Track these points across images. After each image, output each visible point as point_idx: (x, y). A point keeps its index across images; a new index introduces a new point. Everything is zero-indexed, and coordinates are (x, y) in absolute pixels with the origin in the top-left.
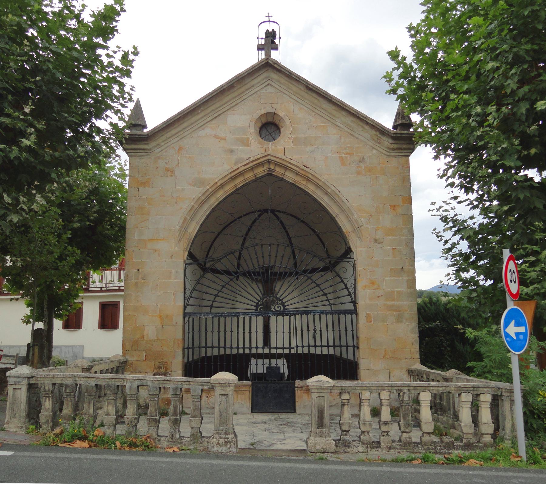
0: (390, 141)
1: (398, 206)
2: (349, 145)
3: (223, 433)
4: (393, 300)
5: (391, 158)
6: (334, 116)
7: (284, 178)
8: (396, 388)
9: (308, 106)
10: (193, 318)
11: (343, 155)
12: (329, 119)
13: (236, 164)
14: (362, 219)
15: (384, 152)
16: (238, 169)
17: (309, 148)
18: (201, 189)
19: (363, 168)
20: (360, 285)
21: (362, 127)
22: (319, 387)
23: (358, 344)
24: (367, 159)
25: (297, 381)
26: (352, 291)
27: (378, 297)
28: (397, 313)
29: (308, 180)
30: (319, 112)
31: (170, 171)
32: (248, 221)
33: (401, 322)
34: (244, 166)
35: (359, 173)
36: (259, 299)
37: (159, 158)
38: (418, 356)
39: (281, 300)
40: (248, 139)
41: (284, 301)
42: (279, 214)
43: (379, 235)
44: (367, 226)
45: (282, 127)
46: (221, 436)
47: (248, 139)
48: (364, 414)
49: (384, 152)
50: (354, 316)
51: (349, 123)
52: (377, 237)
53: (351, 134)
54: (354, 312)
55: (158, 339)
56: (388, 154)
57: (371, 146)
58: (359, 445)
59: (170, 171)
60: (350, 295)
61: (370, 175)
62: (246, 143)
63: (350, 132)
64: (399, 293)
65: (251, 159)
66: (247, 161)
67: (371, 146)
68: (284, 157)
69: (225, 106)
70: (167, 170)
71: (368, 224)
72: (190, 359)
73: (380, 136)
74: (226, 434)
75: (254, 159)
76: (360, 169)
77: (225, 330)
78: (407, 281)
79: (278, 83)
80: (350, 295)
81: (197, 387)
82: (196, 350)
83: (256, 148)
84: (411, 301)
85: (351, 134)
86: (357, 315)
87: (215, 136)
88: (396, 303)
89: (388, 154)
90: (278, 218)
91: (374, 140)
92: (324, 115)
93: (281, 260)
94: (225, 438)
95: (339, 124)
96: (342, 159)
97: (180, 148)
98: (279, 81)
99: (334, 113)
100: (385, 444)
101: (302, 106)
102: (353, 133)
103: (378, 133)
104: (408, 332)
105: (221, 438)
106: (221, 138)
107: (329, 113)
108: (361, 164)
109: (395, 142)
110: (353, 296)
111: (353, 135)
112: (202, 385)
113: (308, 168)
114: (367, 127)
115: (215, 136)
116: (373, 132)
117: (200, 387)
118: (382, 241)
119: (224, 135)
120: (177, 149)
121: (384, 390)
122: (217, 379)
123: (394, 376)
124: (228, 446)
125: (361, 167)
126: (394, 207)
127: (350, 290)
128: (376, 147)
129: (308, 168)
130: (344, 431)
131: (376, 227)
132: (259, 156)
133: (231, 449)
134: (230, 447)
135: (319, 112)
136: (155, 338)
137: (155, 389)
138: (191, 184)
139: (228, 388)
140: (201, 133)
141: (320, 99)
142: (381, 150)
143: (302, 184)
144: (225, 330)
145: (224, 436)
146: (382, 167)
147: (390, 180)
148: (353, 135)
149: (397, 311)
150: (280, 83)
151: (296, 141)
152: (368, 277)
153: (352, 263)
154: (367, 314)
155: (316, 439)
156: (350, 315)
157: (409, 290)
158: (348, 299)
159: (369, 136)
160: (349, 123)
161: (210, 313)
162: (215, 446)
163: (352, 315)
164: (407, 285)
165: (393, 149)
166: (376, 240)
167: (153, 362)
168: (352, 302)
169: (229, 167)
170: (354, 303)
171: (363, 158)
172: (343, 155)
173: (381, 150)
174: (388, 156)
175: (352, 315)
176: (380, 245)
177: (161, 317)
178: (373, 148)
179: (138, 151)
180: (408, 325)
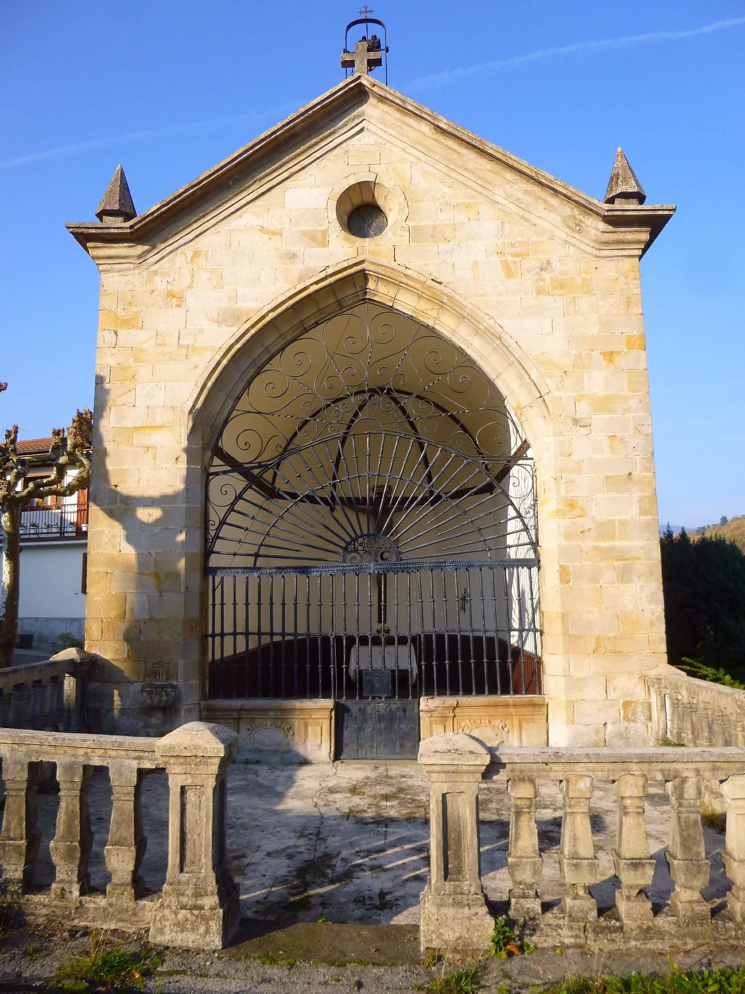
0: (602, 226)
1: (619, 353)
2: (519, 239)
3: (189, 892)
4: (613, 538)
5: (603, 261)
6: (490, 183)
7: (396, 307)
8: (660, 766)
9: (439, 166)
10: (222, 578)
11: (509, 258)
12: (480, 189)
13: (300, 279)
14: (548, 381)
15: (589, 249)
16: (305, 289)
17: (443, 246)
18: (235, 329)
19: (548, 281)
20: (544, 511)
21: (545, 201)
22: (451, 768)
23: (542, 625)
24: (556, 265)
25: (423, 700)
26: (530, 523)
27: (582, 532)
28: (620, 563)
29: (441, 305)
30: (461, 178)
31: (175, 298)
32: (345, 410)
33: (629, 581)
34: (317, 283)
35: (539, 292)
36: (348, 540)
37: (155, 273)
38: (663, 648)
39: (362, 535)
40: (325, 233)
41: (359, 533)
42: (404, 400)
43: (583, 410)
44: (558, 394)
45: (390, 210)
46: (184, 900)
47: (325, 233)
48: (575, 839)
49: (589, 249)
50: (534, 570)
51: (520, 195)
52: (578, 416)
53: (523, 217)
54: (534, 563)
55: (152, 619)
56: (597, 253)
57: (562, 240)
58: (561, 922)
59: (175, 298)
60: (526, 529)
61: (562, 295)
62: (320, 239)
63: (522, 212)
64: (623, 523)
65: (330, 271)
66: (323, 275)
67: (562, 240)
68: (393, 265)
69: (280, 171)
70: (171, 295)
71: (559, 389)
72: (218, 656)
73: (581, 217)
74: (197, 894)
75: (337, 268)
76: (541, 283)
77: (284, 601)
78: (640, 501)
79: (381, 126)
80: (526, 529)
81: (127, 762)
82: (229, 640)
83: (340, 251)
84: (649, 540)
85: (523, 217)
86: (539, 568)
87: (262, 229)
88: (617, 543)
89: (597, 253)
90: (397, 402)
91: (568, 226)
92: (468, 183)
93: (405, 481)
94: (195, 907)
95: (499, 199)
96: (506, 265)
97: (196, 254)
98: (383, 122)
99: (490, 177)
100: (634, 920)
101: (427, 167)
102: (526, 215)
103: (576, 212)
104: (644, 600)
105: (184, 907)
106: (273, 233)
107: (481, 178)
108: (543, 274)
109: (611, 228)
110: (533, 533)
111: (526, 220)
112: (139, 758)
113: (440, 283)
114: (554, 201)
115: (262, 229)
116: (568, 210)
117: (135, 765)
118: (588, 422)
119: (280, 227)
120: (190, 254)
121: (629, 772)
122: (171, 748)
123: (615, 689)
124: (202, 929)
125: (543, 280)
126: (610, 356)
127: (526, 521)
128: (573, 241)
129: (440, 283)
130: (520, 883)
131: (575, 394)
132: (346, 264)
133: (208, 938)
134: (207, 932)
135: (461, 178)
136: (147, 617)
137: (19, 768)
138: (213, 321)
139: (202, 770)
140: (235, 222)
141: (464, 151)
142: (583, 247)
143: (429, 315)
144: (284, 601)
145: (191, 902)
146: (585, 280)
147: (601, 303)
148: (526, 220)
149: (620, 560)
150: (385, 125)
151: (415, 234)
152: (563, 493)
153: (528, 468)
154: (561, 566)
155: (443, 910)
156: (525, 570)
157: (643, 518)
158: (524, 538)
159: (559, 219)
160: (520, 195)
161: (255, 568)
162: (167, 930)
163: (530, 569)
164: (640, 507)
165: (607, 243)
166: (576, 421)
167: (143, 664)
168: (531, 543)
169: (288, 286)
170: (535, 545)
171: (549, 263)
172: (509, 258)
173: (583, 247)
174: (598, 257)
175: (530, 569)
176: (584, 431)
177: (157, 575)
178: (566, 242)
179: (118, 261)
180: (642, 587)
